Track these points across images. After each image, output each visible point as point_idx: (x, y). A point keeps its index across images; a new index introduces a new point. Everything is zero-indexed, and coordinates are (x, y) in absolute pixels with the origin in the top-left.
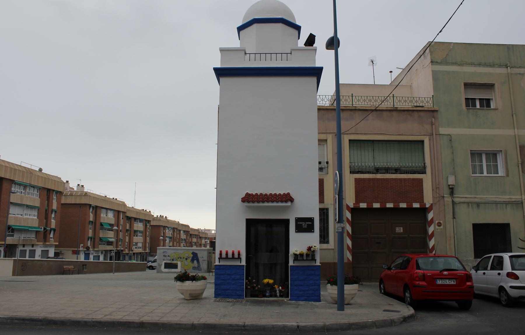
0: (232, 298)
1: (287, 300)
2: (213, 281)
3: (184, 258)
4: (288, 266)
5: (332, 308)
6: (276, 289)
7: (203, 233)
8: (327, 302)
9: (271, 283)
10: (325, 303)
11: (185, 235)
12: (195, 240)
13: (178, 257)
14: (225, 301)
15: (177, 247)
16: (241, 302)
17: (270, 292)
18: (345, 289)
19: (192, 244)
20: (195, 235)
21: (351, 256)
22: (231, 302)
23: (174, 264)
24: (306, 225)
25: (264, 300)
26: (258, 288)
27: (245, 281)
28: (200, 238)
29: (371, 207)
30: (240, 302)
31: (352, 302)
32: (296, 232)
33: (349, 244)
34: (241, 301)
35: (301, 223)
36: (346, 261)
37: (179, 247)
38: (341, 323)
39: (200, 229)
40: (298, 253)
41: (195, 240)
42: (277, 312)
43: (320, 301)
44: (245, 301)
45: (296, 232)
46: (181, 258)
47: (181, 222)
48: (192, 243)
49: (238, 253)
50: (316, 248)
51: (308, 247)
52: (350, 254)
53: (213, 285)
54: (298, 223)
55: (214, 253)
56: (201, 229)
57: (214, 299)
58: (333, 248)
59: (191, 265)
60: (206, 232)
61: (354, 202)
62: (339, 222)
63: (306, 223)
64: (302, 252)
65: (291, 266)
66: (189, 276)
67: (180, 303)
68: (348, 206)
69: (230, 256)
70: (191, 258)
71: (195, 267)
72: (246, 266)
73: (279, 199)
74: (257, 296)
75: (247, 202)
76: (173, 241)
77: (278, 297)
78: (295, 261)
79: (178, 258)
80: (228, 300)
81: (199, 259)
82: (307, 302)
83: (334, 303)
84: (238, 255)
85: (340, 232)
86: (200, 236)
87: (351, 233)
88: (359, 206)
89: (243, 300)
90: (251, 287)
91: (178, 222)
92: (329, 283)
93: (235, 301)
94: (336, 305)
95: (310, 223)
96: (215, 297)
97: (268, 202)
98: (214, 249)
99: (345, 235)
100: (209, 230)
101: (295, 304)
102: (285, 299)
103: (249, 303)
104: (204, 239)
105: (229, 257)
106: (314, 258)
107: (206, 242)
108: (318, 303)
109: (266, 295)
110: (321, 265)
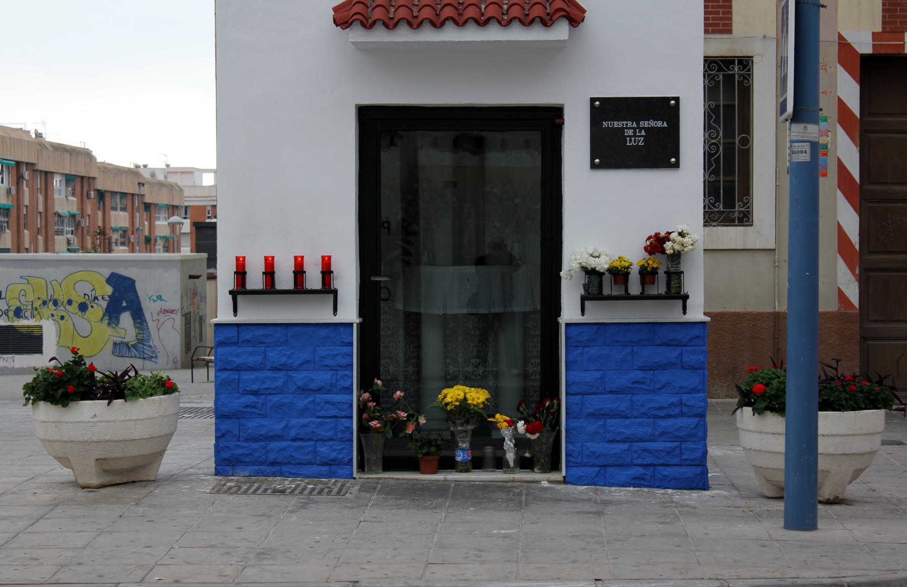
0: (296, 475)
1: (550, 482)
2: (210, 404)
3: (70, 302)
4: (557, 324)
5: (758, 517)
6: (499, 429)
7: (161, 185)
8: (735, 492)
9: (476, 405)
10: (726, 493)
11: (71, 198)
12: (120, 219)
13: (44, 297)
14: (264, 487)
15: (36, 251)
16: (338, 493)
17: (473, 447)
18: (821, 431)
19: (110, 239)
20: (123, 195)
21: (857, 283)
22: (292, 492)
23: (23, 330)
24: (643, 133)
25: (445, 480)
26: (418, 428)
27: (359, 396)
28: (148, 207)
30: (336, 490)
31: (852, 490)
32: (593, 166)
34: (340, 490)
35: (617, 124)
36: (827, 304)
37: (46, 250)
38: (799, 581)
39: (145, 166)
40: (602, 264)
41: (120, 219)
42: (506, 536)
43: (705, 487)
44: (357, 488)
45: (593, 166)
46: (55, 303)
47: (51, 137)
48: (109, 233)
49: (320, 268)
50: (686, 240)
51: (649, 238)
52: (853, 271)
53: (208, 420)
54: (605, 124)
55: (212, 277)
56: (150, 166)
57: (213, 480)
58: (772, 246)
59: (106, 334)
60: (172, 179)
61: (879, 28)
62: (797, 117)
63: (643, 124)
65: (567, 325)
66: (92, 376)
67: (54, 505)
68: (844, 46)
69: (285, 279)
70: (104, 304)
71: (126, 344)
72: (361, 326)
73: (516, 11)
74: (412, 465)
75: (364, 25)
76: (18, 225)
77: (508, 466)
78: (587, 303)
79: (45, 303)
80: (278, 483)
81: (143, 305)
82: (646, 490)
83: (767, 493)
84: (320, 276)
85: (800, 164)
86: (148, 200)
87: (857, 176)
89: (348, 485)
90: (385, 426)
91: (39, 135)
92: (748, 405)
93: (313, 489)
94: (780, 506)
95: (659, 124)
96: (217, 473)
97: (460, 23)
98: (212, 261)
99: (828, 186)
100: (188, 172)
101: (589, 500)
102: (544, 479)
103: (375, 497)
104: (163, 215)
105: (279, 286)
107: (173, 226)
108: (695, 495)
109: (453, 459)
110: (708, 319)
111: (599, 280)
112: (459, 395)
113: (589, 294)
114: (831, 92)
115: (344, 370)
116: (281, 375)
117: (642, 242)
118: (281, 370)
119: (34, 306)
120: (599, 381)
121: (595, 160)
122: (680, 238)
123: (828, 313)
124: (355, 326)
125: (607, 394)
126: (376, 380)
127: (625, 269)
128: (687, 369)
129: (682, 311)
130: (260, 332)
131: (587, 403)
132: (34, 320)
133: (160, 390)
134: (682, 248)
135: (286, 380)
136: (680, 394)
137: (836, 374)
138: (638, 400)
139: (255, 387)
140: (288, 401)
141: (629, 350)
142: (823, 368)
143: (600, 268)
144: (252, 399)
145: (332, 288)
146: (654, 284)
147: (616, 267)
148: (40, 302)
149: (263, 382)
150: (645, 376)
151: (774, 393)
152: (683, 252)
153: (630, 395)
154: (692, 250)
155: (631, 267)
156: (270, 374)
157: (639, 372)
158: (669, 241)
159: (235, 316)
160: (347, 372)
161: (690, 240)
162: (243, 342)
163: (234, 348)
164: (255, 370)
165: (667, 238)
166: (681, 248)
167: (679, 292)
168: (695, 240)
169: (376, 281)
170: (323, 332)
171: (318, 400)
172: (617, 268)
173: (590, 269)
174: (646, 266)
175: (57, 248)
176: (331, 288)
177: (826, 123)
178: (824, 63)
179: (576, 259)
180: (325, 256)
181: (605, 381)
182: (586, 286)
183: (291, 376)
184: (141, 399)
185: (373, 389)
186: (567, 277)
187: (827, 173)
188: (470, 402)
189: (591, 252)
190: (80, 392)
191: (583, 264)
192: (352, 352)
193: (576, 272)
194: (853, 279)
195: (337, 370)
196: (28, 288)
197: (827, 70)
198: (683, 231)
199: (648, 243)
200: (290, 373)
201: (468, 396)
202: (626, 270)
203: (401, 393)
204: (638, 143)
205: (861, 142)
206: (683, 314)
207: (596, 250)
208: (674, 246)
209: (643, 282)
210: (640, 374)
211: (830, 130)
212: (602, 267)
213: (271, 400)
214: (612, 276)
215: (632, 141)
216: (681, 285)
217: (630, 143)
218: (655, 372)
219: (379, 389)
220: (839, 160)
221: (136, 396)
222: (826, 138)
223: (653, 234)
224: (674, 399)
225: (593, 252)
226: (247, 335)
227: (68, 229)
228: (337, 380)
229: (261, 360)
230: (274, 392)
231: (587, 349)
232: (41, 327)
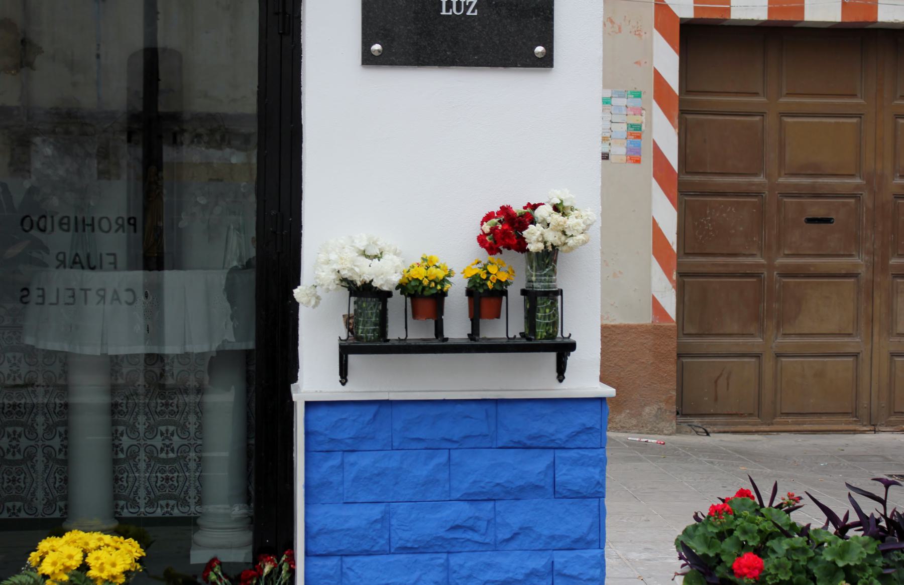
4: (290, 406)
29: (791, 17)
32: (368, 60)
33: (661, 225)
45: (368, 60)
50: (571, 221)
52: (670, 278)
64: (427, 262)
65: (309, 405)
78: (353, 359)
88: (728, 10)
106: (554, 323)
111: (380, 307)
112: (70, 557)
113: (358, 338)
114: (646, 62)
117: (474, 228)
120: (378, 526)
121: (373, 45)
122: (557, 217)
123: (641, 326)
125: (393, 553)
127: (436, 284)
128: (565, 497)
129: (556, 374)
131: (351, 574)
134: (563, 238)
136: (550, 552)
137: (883, 514)
138: (461, 566)
141: (442, 458)
142: (850, 495)
143: (382, 282)
146: (498, 317)
147: (417, 279)
150: (477, 514)
151: (787, 578)
152: (565, 248)
153: (445, 556)
154: (584, 243)
155: (448, 278)
157: (465, 506)
158: (533, 222)
161: (580, 221)
165: (527, 219)
166: (560, 239)
167: (552, 336)
168: (589, 222)
172: (421, 282)
173: (359, 284)
174: (484, 277)
177: (639, 99)
178: (638, 28)
179: (328, 262)
181: (390, 525)
182: (351, 321)
186: (309, 302)
187: (640, 158)
188: (93, 573)
189: (361, 245)
191: (346, 274)
193: (328, 290)
194: (670, 286)
197: (642, 36)
198: (562, 201)
199: (487, 228)
201: (90, 560)
202: (439, 287)
204: (465, 12)
205: (680, 123)
206: (557, 381)
207: (375, 243)
208: (545, 236)
209: (475, 318)
210: (464, 511)
211: (644, 107)
212: (387, 281)
214: (409, 299)
215: (452, 8)
216: (558, 320)
217: (447, 11)
218: (498, 503)
220: (654, 142)
222: (640, 116)
223: (496, 209)
224: (538, 562)
225: (368, 245)
231: (352, 457)
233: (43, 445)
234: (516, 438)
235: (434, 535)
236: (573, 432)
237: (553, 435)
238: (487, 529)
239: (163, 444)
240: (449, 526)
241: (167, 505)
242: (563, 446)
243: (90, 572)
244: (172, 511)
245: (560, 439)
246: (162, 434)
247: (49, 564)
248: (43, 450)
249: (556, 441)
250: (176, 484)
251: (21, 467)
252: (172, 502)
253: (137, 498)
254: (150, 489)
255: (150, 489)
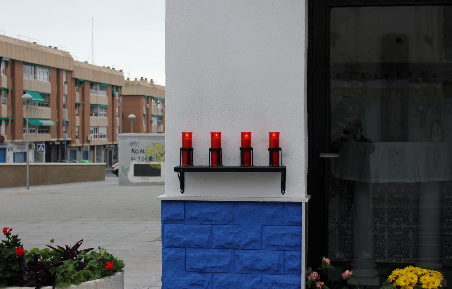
23: (152, 166)
27: (307, 275)
49: (267, 145)
72: (309, 204)
112: (412, 278)
115: (293, 250)
116: (227, 254)
118: (227, 248)
119: (157, 156)
124: (304, 206)
126: (324, 258)
130: (207, 209)
132: (157, 162)
133: (99, 273)
135: (233, 259)
139: (201, 265)
140: (235, 280)
144: (198, 277)
145: (280, 165)
148: (160, 154)
149: (209, 261)
150: (203, 279)
156: (216, 252)
159: (182, 193)
160: (295, 253)
162: (190, 219)
163: (180, 225)
164: (202, 248)
169: (325, 158)
170: (271, 211)
171: (265, 281)
175: (153, 130)
176: (279, 166)
180: (273, 133)
183: (237, 255)
184: (73, 286)
185: (321, 267)
190: (6, 278)
192: (301, 232)
195: (284, 250)
196: (155, 148)
200: (237, 252)
201: (422, 280)
203: (350, 272)
213: (217, 279)
219: (327, 267)
221: (67, 282)
226: (194, 212)
227: (101, 113)
228: (285, 261)
229: (207, 238)
230: (221, 271)
232: (160, 165)
233: (338, 226)
234: (221, 244)
235: (183, 288)
236: (247, 242)
237: (238, 243)
238: (208, 286)
239: (397, 227)
240: (190, 283)
241: (399, 257)
242: (243, 248)
243: (423, 286)
244: (401, 260)
245: (241, 245)
246: (396, 222)
247: (403, 281)
248: (338, 229)
249: (240, 246)
250: (403, 247)
251: (395, 251)
252: (401, 256)
253: (408, 254)
254: (390, 248)
255: (390, 248)
